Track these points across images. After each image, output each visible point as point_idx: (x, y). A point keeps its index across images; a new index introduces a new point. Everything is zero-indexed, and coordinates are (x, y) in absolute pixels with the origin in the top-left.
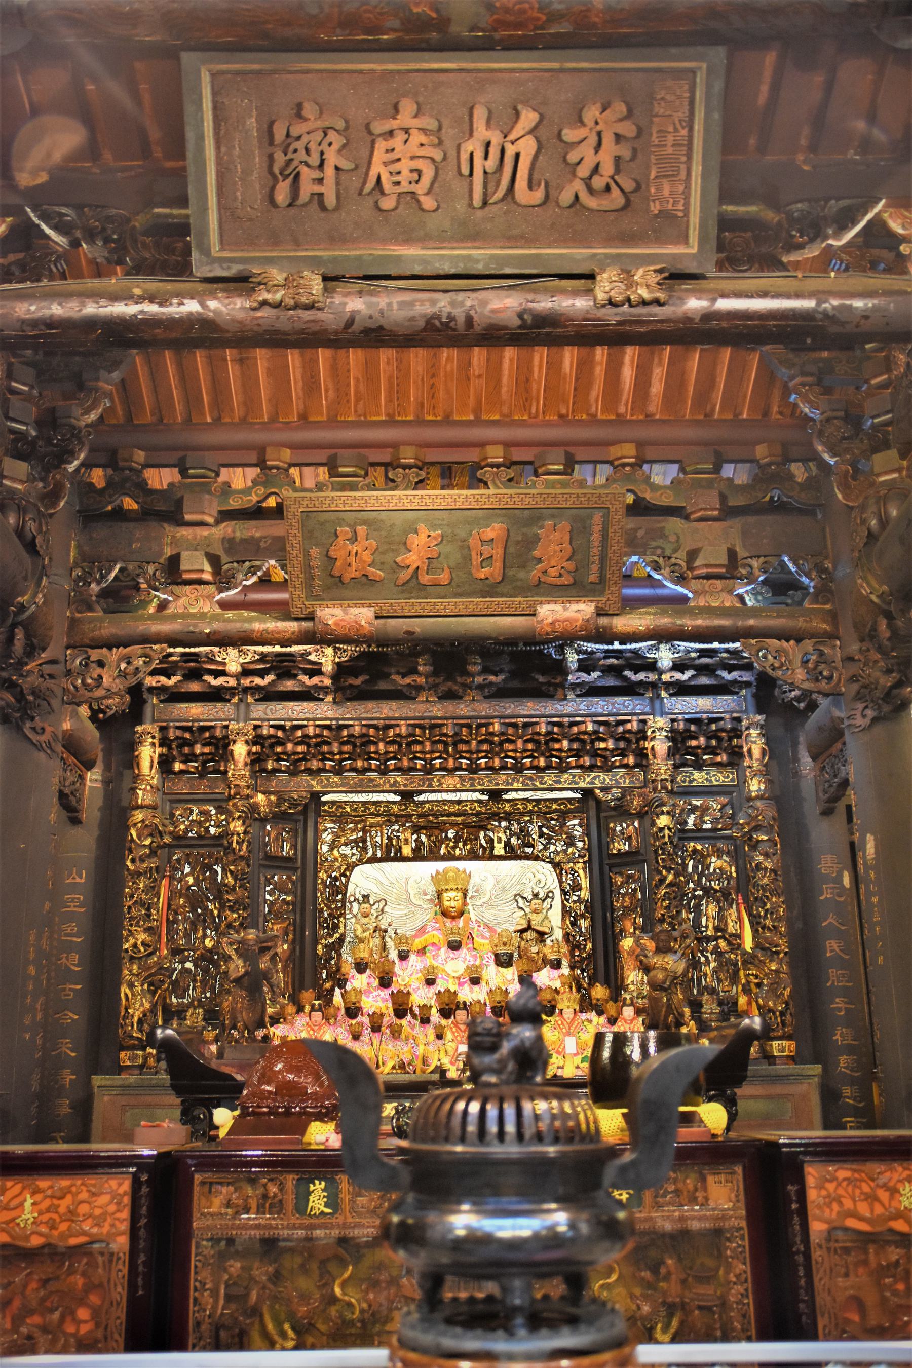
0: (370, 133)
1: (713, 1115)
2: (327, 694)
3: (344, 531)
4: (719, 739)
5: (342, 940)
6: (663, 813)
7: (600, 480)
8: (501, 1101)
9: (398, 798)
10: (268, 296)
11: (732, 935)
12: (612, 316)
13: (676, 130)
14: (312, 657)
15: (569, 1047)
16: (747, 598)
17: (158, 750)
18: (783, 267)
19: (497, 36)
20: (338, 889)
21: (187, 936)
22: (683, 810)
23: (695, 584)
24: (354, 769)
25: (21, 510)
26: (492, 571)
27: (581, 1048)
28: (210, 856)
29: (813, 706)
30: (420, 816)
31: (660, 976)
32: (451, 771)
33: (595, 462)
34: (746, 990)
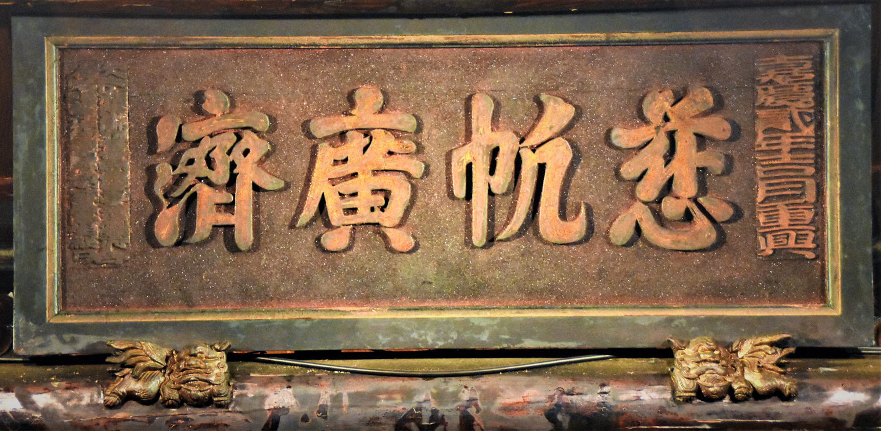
13: (795, 128)
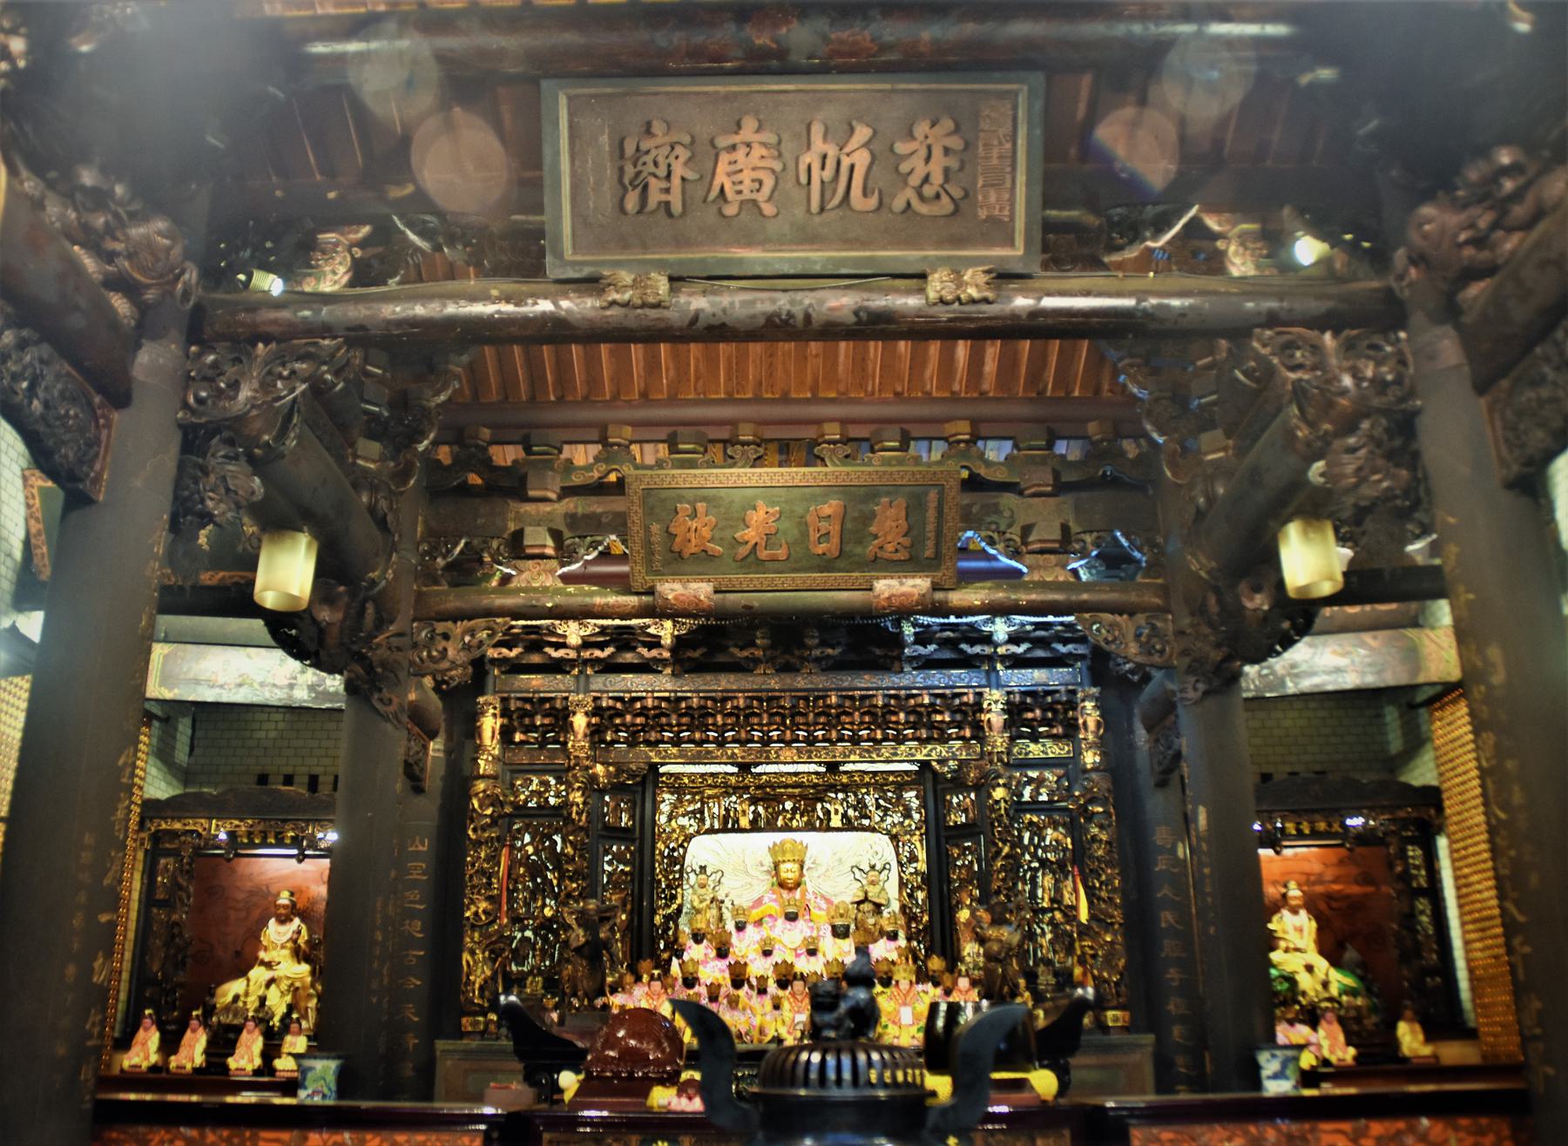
0: (714, 146)
1: (1043, 1081)
2: (665, 666)
3: (684, 507)
4: (1055, 712)
5: (679, 910)
7: (936, 456)
8: (838, 1053)
9: (735, 770)
10: (617, 297)
11: (1068, 907)
12: (944, 314)
13: (1000, 144)
14: (651, 630)
15: (903, 1017)
16: (1081, 572)
17: (499, 721)
18: (1105, 267)
19: (832, 63)
20: (676, 861)
21: (527, 905)
22: (1019, 782)
23: (1029, 559)
24: (690, 741)
25: (374, 489)
26: (829, 547)
27: (916, 1017)
28: (550, 826)
29: (1146, 678)
30: (758, 787)
31: (995, 947)
32: (788, 743)
33: (931, 439)
34: (1082, 961)
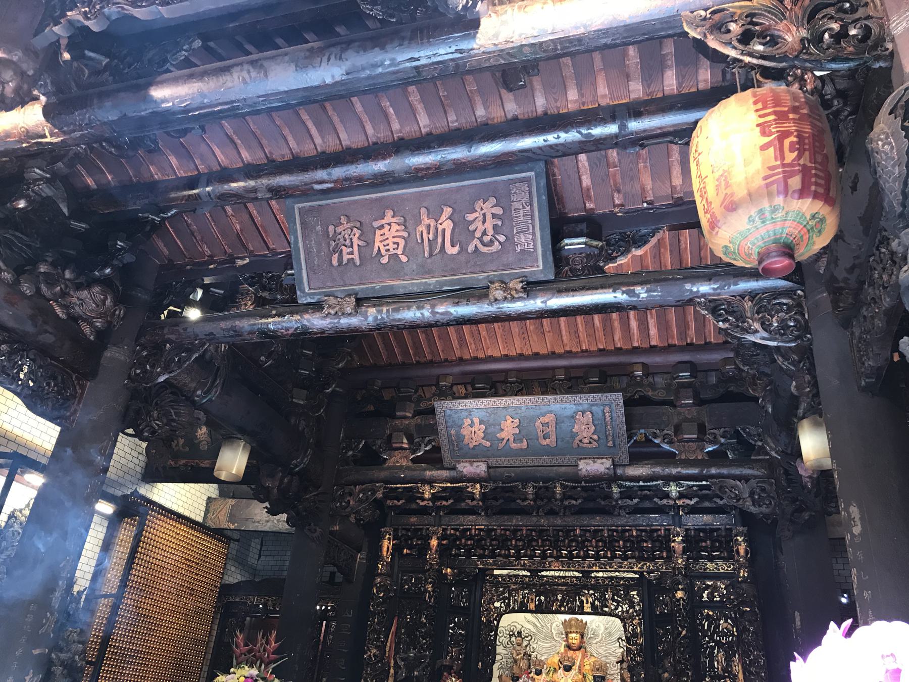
4: (720, 542)
6: (679, 589)
13: (524, 208)
22: (699, 588)
